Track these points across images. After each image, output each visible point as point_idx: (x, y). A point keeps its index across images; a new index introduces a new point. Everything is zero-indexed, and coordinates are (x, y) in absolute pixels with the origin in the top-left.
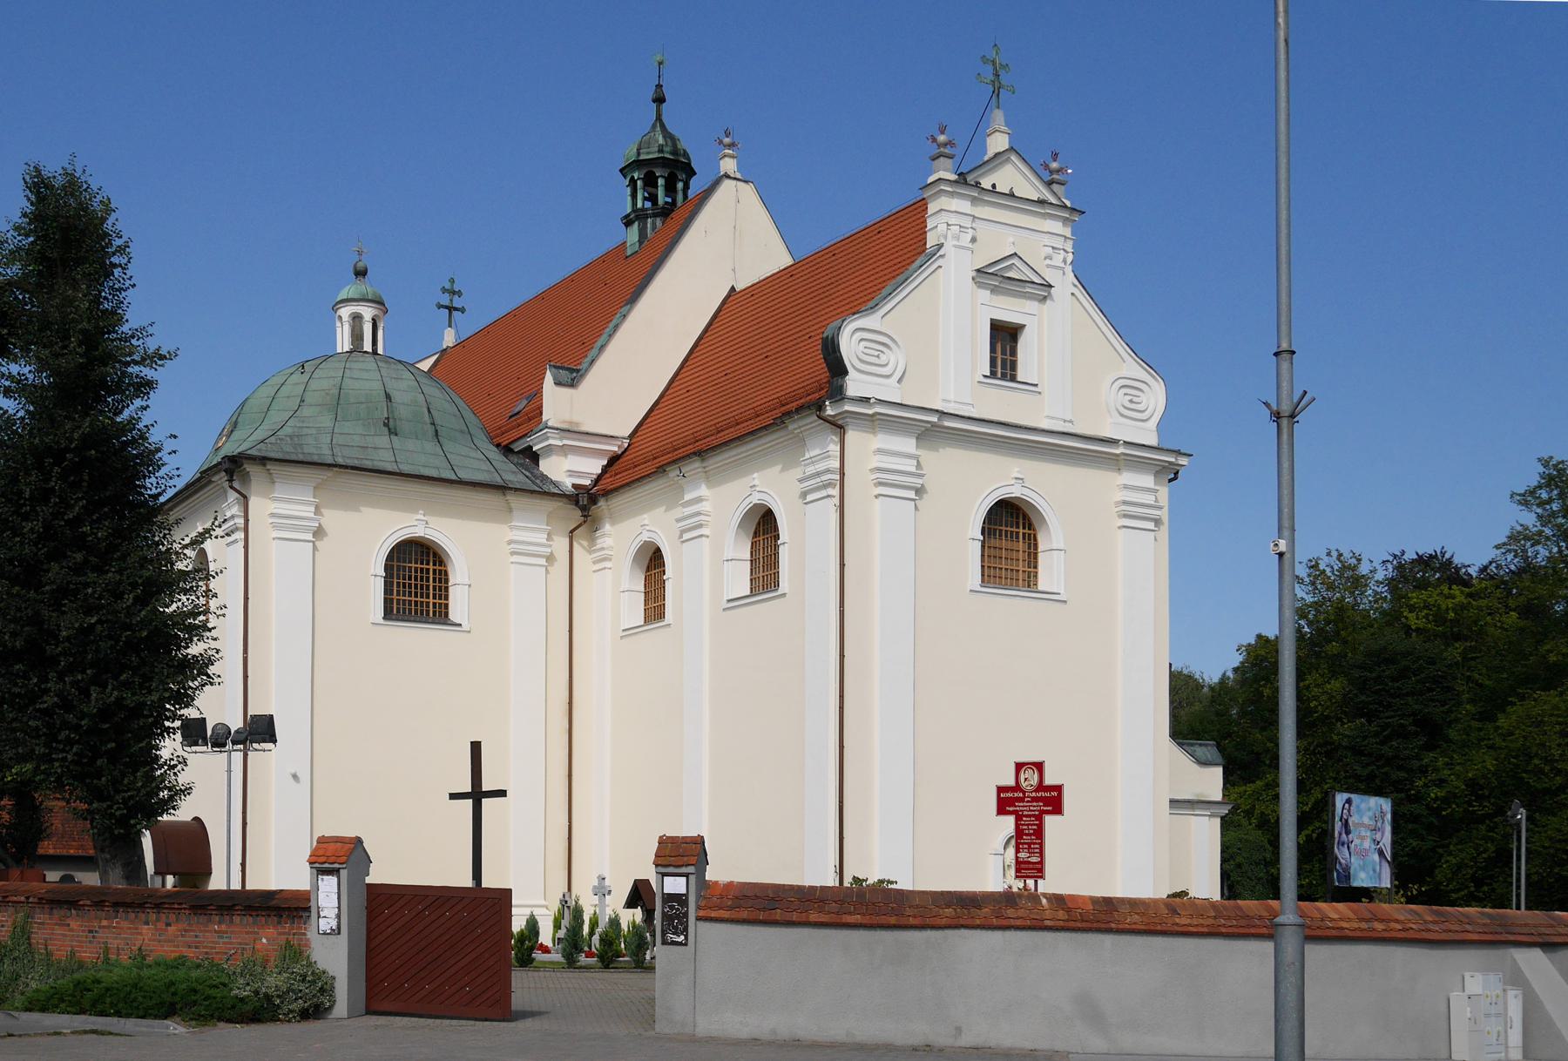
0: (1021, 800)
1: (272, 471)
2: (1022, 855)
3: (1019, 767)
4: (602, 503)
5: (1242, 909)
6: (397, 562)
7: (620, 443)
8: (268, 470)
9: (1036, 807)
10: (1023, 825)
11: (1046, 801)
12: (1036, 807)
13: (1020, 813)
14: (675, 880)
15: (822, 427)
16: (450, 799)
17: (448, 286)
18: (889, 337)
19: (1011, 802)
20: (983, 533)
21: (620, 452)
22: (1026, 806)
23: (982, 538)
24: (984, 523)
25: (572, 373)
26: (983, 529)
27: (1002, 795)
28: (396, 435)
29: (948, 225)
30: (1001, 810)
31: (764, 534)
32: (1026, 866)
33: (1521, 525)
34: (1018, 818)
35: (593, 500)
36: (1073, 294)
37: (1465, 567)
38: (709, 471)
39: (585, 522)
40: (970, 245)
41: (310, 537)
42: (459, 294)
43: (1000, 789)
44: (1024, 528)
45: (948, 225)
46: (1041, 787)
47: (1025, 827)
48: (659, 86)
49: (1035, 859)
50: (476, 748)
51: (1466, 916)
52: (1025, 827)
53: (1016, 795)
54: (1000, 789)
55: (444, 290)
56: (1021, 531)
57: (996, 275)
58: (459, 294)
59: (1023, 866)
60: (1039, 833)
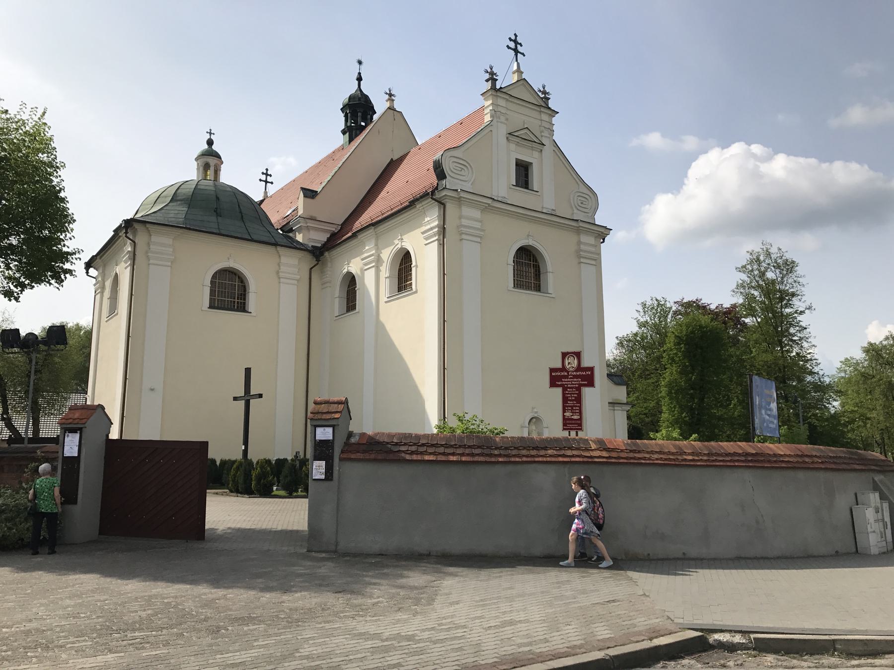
0: (566, 377)
1: (149, 229)
2: (568, 414)
3: (564, 355)
4: (326, 254)
5: (724, 448)
6: (237, 299)
7: (336, 227)
8: (148, 228)
9: (576, 382)
10: (568, 394)
11: (583, 378)
12: (576, 382)
13: (566, 386)
14: (324, 430)
15: (434, 204)
16: (234, 400)
17: (265, 172)
18: (467, 162)
19: (560, 378)
20: (514, 262)
21: (336, 232)
22: (570, 381)
23: (513, 264)
24: (514, 258)
25: (313, 193)
26: (514, 261)
27: (553, 374)
28: (221, 216)
29: (495, 111)
30: (554, 382)
31: (405, 264)
32: (571, 422)
33: (742, 280)
34: (565, 389)
35: (322, 254)
36: (554, 150)
37: (708, 305)
38: (378, 234)
39: (317, 264)
40: (505, 122)
41: (169, 264)
42: (270, 176)
43: (552, 370)
44: (533, 262)
45: (495, 111)
46: (579, 368)
47: (569, 395)
48: (360, 73)
49: (575, 417)
50: (248, 371)
51: (821, 449)
52: (569, 395)
53: (562, 374)
54: (552, 370)
55: (263, 173)
56: (532, 263)
57: (518, 137)
58: (270, 176)
59: (568, 422)
60: (579, 399)
